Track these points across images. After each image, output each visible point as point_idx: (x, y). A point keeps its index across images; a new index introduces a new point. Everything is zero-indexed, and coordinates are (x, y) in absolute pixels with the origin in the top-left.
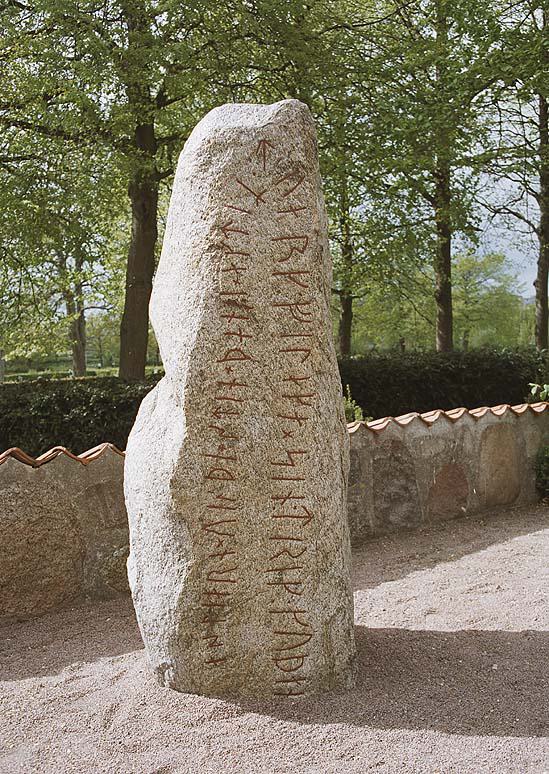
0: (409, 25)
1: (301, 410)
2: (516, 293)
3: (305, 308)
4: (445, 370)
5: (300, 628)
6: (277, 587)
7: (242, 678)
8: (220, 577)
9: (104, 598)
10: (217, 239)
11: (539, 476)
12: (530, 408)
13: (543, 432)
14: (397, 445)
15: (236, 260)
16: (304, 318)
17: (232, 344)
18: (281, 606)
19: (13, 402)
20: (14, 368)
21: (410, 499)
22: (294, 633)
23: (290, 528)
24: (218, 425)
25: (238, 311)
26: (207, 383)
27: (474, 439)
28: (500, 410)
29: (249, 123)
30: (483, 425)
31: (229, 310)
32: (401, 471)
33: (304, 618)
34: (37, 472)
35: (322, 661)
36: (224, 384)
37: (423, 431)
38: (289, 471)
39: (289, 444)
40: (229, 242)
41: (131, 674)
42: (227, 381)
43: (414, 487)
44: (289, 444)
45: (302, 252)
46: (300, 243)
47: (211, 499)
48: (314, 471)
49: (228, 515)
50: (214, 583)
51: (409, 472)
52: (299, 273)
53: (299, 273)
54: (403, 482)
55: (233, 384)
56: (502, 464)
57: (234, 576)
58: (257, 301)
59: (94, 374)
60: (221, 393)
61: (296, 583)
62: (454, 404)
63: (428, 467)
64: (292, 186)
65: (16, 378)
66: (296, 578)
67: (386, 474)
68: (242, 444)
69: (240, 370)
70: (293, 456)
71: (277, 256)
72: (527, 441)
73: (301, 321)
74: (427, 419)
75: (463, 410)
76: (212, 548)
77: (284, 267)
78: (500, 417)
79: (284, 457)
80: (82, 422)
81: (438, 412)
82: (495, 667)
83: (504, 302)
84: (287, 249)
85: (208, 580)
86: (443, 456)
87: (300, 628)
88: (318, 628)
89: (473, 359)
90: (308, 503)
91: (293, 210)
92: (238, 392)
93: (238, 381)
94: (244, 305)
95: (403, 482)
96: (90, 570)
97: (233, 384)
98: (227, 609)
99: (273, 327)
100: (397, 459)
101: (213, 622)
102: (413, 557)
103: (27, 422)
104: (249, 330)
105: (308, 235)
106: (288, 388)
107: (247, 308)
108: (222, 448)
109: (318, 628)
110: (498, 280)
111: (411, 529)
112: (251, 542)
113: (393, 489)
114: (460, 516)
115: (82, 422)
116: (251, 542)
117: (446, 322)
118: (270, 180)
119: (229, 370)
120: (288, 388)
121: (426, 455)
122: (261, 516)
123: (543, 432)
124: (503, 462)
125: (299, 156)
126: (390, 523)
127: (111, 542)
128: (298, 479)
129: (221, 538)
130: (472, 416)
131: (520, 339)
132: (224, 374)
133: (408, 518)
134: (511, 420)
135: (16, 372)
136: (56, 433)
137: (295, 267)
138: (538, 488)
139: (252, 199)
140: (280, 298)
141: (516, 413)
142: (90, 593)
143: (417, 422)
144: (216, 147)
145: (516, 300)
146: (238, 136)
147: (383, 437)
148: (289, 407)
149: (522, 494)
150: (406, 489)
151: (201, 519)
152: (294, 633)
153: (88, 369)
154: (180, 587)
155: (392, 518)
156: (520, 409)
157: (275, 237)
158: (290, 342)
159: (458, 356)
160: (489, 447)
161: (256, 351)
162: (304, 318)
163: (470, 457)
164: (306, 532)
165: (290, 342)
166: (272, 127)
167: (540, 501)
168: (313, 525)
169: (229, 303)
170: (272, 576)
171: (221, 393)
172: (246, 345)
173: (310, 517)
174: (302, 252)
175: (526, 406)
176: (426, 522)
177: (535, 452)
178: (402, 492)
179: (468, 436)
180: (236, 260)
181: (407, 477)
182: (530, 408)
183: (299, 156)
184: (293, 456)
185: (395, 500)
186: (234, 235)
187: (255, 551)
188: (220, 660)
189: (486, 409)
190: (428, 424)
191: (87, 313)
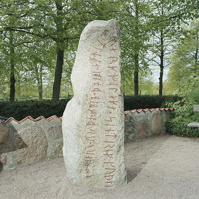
0: (129, 11)
1: (114, 106)
2: (153, 81)
3: (116, 77)
4: (137, 100)
5: (112, 168)
6: (106, 156)
7: (95, 182)
8: (90, 153)
9: (53, 159)
10: (92, 57)
11: (167, 127)
12: (164, 109)
13: (167, 116)
14: (131, 118)
15: (97, 63)
16: (116, 80)
17: (96, 86)
18: (107, 162)
19: (24, 106)
20: (23, 98)
21: (134, 132)
22: (111, 169)
23: (110, 139)
24: (91, 109)
25: (98, 78)
26: (88, 97)
27: (150, 117)
28: (157, 109)
29: (102, 25)
30: (153, 113)
31: (95, 77)
32: (132, 125)
33: (113, 165)
34: (36, 123)
35: (118, 177)
36: (93, 98)
37: (137, 114)
38: (111, 123)
39: (111, 115)
40: (95, 58)
41: (62, 180)
42: (94, 97)
43: (135, 129)
44: (111, 115)
45: (116, 61)
46: (115, 59)
47: (88, 131)
48: (117, 123)
49: (93, 135)
50: (88, 154)
51: (134, 125)
52: (115, 67)
53: (115, 67)
54: (132, 128)
55: (95, 98)
56: (157, 123)
57: (94, 152)
58: (103, 74)
59: (44, 99)
60: (92, 100)
61: (111, 155)
62: (139, 108)
63: (139, 124)
64: (113, 43)
65: (24, 100)
66: (111, 153)
67: (128, 126)
68: (98, 115)
69: (98, 94)
70: (112, 119)
71: (109, 62)
72: (164, 118)
73: (115, 81)
74: (139, 111)
75: (148, 109)
76: (88, 145)
77: (111, 65)
78: (157, 111)
79: (109, 119)
80: (42, 111)
81: (142, 109)
82: (164, 179)
83: (150, 83)
84: (112, 61)
85: (87, 153)
86: (143, 121)
87: (112, 168)
88: (117, 168)
89: (144, 97)
90: (115, 132)
91: (113, 50)
92: (97, 100)
93: (97, 97)
94: (99, 76)
95: (132, 128)
96: (49, 151)
97: (95, 98)
98: (92, 162)
99: (107, 82)
100: (131, 122)
101: (87, 166)
102: (136, 148)
103: (27, 111)
104: (100, 83)
105: (118, 57)
106: (111, 100)
107: (100, 76)
108: (92, 116)
109: (117, 168)
110: (149, 78)
111: (134, 141)
112: (99, 143)
113: (130, 130)
114: (146, 138)
115: (42, 111)
116: (99, 143)
117: (136, 88)
118: (107, 41)
119: (94, 94)
120: (111, 100)
121: (138, 121)
122: (102, 135)
123: (167, 116)
124: (158, 123)
125: (116, 35)
126: (129, 139)
127: (55, 143)
128: (113, 125)
129: (91, 142)
130: (150, 111)
131: (154, 93)
132: (93, 95)
133: (133, 138)
134: (160, 112)
135: (23, 99)
136: (35, 114)
137: (114, 66)
138: (166, 130)
139: (102, 46)
140: (110, 74)
141: (161, 110)
142: (49, 157)
143: (136, 112)
144: (92, 31)
145: (153, 83)
146: (98, 29)
147: (127, 115)
148: (111, 105)
149: (162, 132)
150: (133, 130)
151: (85, 136)
152: (111, 169)
153: (43, 98)
154: (79, 156)
155: (129, 138)
156: (162, 109)
157: (109, 57)
158: (112, 87)
159: (140, 96)
160: (154, 118)
161: (102, 89)
162: (116, 80)
163: (149, 121)
164: (114, 140)
165: (112, 87)
166: (108, 26)
167: (167, 134)
168: (117, 138)
169: (95, 75)
170: (105, 153)
171: (92, 100)
172: (100, 87)
173: (116, 136)
174: (116, 61)
175: (164, 108)
176: (138, 139)
177: (165, 121)
178: (132, 131)
179: (149, 116)
180: (97, 63)
181: (133, 127)
182: (164, 109)
183: (116, 35)
184: (112, 119)
185: (130, 133)
186: (97, 56)
187: (100, 145)
188: (89, 176)
189: (153, 109)
190: (139, 113)
191: (43, 83)
